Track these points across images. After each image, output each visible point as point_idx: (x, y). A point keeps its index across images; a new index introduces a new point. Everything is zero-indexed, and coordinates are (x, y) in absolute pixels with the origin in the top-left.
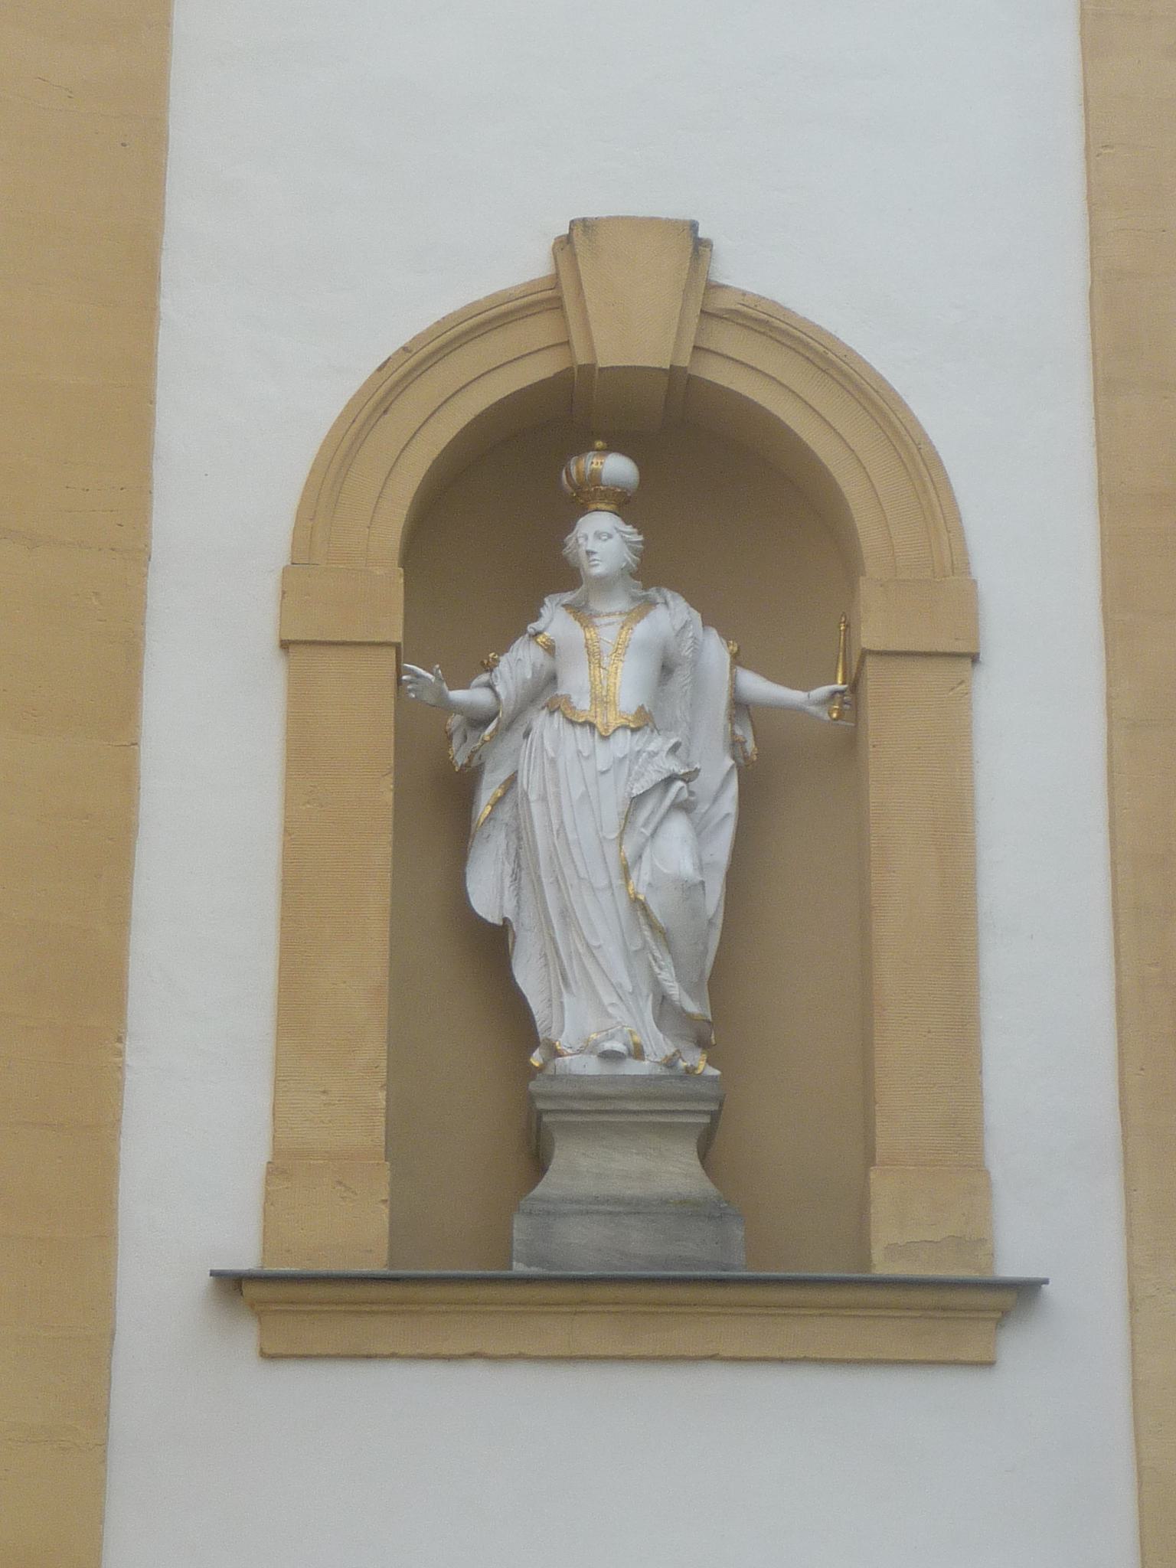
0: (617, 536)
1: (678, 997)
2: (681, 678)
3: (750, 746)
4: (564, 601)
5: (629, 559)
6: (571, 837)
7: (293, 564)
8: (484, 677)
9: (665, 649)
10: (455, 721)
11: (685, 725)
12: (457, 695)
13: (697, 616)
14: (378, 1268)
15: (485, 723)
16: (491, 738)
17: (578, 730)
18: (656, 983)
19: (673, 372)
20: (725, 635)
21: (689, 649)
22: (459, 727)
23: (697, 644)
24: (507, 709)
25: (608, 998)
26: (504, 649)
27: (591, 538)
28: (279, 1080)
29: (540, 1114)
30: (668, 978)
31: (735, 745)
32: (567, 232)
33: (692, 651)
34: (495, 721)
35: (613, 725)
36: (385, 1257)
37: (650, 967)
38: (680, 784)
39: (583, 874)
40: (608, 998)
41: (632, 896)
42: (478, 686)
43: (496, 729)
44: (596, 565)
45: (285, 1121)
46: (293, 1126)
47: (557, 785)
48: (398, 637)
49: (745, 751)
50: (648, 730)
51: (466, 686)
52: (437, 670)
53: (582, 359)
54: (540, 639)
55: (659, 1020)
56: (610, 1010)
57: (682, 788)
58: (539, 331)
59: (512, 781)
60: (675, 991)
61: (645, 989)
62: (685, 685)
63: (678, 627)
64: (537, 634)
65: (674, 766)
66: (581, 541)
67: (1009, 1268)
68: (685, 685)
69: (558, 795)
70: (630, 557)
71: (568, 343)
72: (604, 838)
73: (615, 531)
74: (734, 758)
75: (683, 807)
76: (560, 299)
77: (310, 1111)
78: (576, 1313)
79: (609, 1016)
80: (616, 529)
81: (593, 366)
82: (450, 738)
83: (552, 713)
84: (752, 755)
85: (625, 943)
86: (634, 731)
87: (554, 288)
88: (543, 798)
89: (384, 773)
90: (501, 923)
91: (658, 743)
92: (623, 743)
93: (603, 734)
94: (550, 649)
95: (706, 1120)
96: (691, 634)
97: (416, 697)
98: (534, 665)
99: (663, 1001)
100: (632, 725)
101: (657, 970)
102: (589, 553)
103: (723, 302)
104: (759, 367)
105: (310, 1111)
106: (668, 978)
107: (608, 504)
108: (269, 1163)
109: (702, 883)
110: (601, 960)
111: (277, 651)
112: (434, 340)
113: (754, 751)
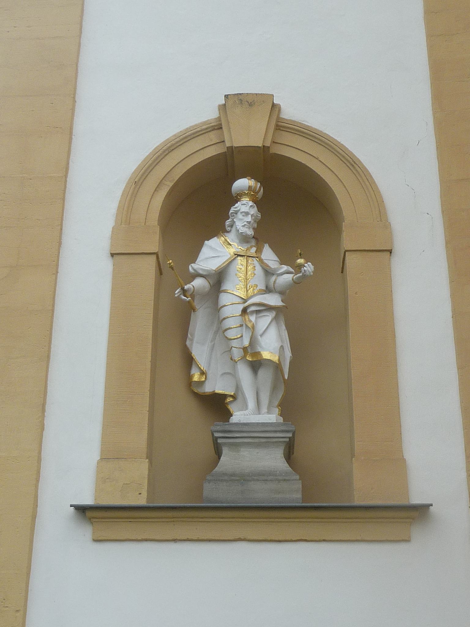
14: (142, 501)
19: (265, 148)
29: (217, 438)
53: (228, 144)
58: (213, 137)
67: (416, 500)
71: (224, 141)
76: (221, 124)
104: (289, 145)
111: (110, 258)
112: (339, 148)
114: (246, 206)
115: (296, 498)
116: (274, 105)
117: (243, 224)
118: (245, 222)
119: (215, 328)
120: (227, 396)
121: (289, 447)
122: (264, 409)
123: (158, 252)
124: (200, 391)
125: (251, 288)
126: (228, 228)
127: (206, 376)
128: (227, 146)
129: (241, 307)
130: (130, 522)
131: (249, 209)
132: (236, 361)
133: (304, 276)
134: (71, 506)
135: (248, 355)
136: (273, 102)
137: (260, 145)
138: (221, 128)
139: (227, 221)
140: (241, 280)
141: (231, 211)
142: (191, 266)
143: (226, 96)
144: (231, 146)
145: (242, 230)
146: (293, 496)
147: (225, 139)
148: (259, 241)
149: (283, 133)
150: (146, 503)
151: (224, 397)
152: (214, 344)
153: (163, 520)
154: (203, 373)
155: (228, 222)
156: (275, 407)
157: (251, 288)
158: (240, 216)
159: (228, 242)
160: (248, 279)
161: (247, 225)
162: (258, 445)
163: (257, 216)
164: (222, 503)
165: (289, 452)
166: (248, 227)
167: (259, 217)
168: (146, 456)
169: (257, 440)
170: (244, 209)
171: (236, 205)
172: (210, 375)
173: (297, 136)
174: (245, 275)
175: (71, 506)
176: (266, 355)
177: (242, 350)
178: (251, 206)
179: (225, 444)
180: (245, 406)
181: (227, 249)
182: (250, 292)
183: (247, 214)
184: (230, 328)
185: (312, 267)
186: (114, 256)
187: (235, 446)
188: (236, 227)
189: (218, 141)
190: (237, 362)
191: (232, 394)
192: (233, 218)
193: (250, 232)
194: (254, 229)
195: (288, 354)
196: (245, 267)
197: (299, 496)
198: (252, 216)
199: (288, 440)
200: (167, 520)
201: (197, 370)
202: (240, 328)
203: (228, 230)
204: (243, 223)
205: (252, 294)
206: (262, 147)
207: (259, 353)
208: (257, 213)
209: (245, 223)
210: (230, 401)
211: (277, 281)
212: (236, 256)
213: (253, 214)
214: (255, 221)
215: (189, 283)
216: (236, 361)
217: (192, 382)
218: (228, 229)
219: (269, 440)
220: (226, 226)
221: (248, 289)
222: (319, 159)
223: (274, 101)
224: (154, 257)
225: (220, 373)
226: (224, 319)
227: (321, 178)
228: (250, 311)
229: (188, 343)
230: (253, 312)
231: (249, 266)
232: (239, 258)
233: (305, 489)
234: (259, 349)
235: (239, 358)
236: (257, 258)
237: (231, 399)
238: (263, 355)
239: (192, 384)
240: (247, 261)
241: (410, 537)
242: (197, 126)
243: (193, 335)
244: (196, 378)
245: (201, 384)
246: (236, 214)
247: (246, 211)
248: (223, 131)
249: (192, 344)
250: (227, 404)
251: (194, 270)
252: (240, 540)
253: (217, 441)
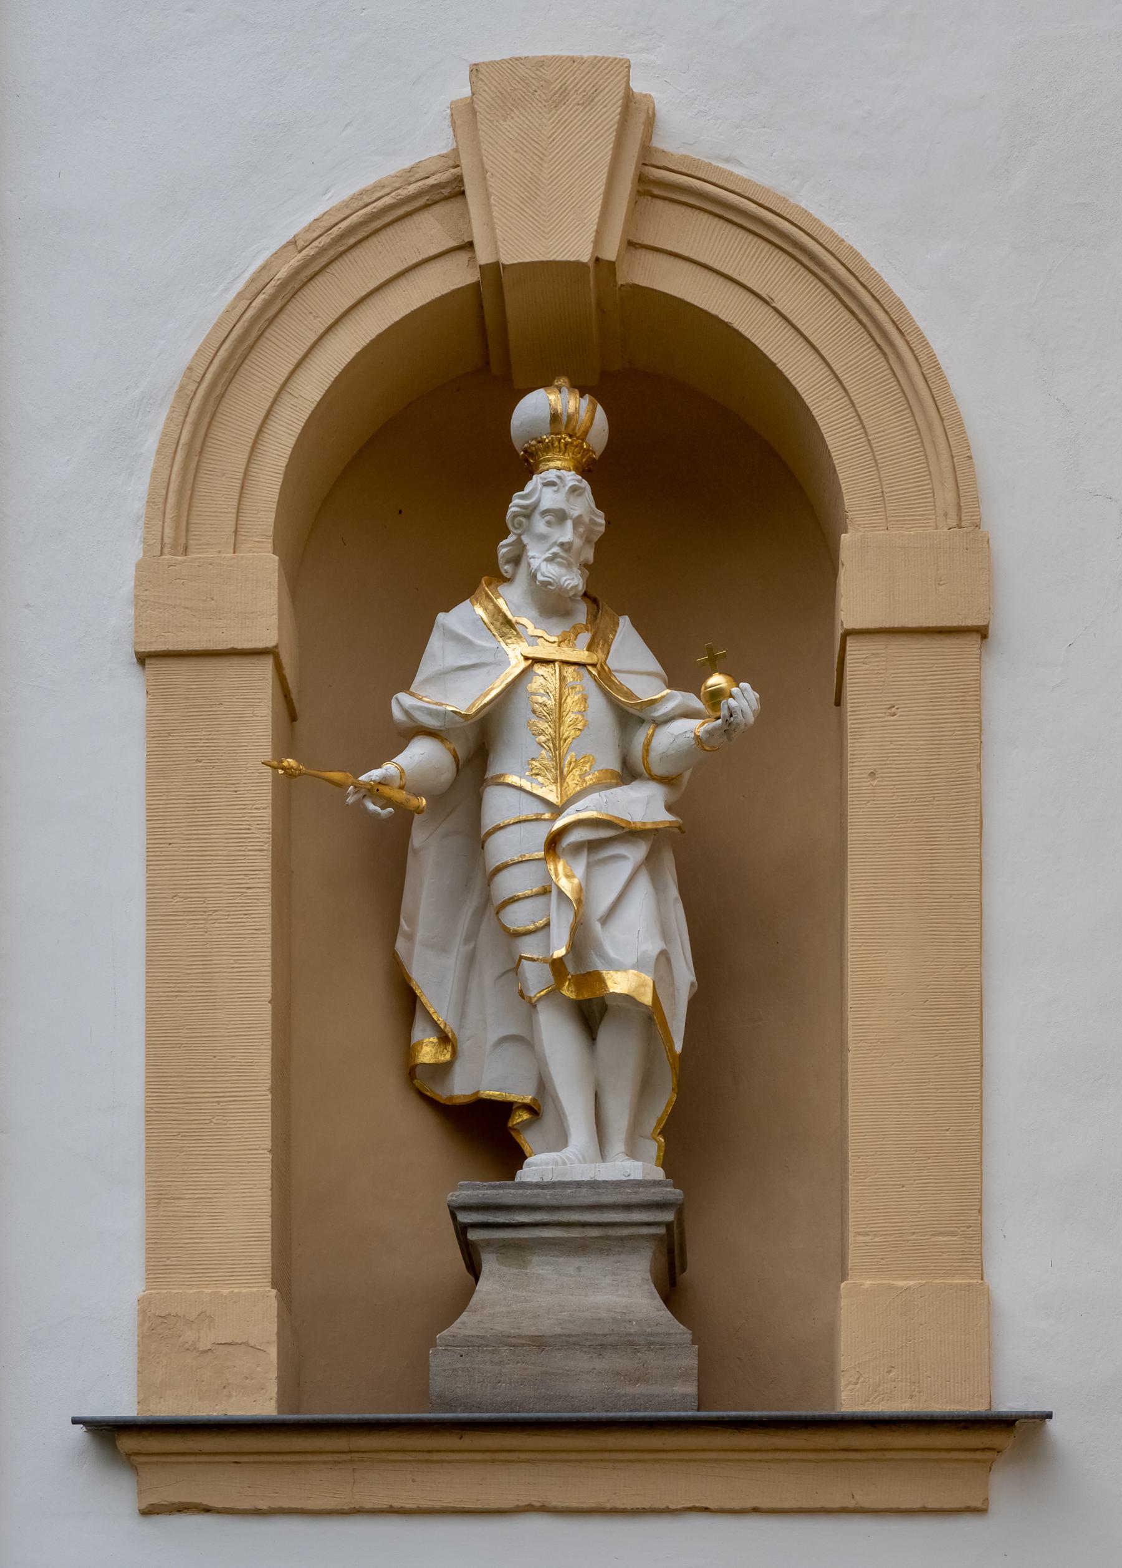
14: (266, 1407)
53: (484, 256)
67: (1008, 1404)
76: (459, 179)
111: (137, 669)
114: (555, 488)
115: (682, 1394)
116: (629, 101)
117: (548, 555)
118: (554, 544)
119: (473, 901)
120: (514, 1107)
121: (670, 1251)
122: (617, 1144)
123: (276, 647)
124: (441, 1093)
125: (573, 768)
126: (506, 567)
127: (453, 1046)
128: (482, 263)
129: (541, 833)
130: (236, 1465)
131: (568, 500)
132: (534, 1000)
133: (729, 728)
134: (75, 1421)
135: (565, 982)
136: (628, 88)
137: (585, 258)
138: (463, 193)
139: (501, 544)
140: (545, 743)
141: (512, 509)
142: (397, 699)
143: (475, 69)
145: (549, 571)
146: (673, 1390)
147: (473, 237)
148: (600, 606)
149: (660, 204)
151: (505, 1108)
152: (475, 947)
153: (325, 1458)
154: (445, 1039)
155: (504, 549)
156: (648, 1138)
157: (573, 768)
158: (540, 525)
159: (505, 616)
160: (565, 740)
161: (562, 557)
162: (581, 1248)
163: (593, 522)
164: (480, 1409)
165: (671, 1265)
166: (564, 561)
167: (601, 525)
168: (270, 1280)
169: (575, 1233)
170: (550, 499)
171: (529, 487)
172: (465, 1046)
173: (705, 217)
174: (557, 724)
175: (75, 1421)
176: (619, 983)
177: (547, 968)
178: (574, 490)
179: (488, 1243)
180: (562, 1140)
181: (500, 639)
182: (573, 783)
183: (560, 516)
184: (513, 900)
185: (753, 696)
187: (516, 1251)
188: (529, 565)
189: (453, 244)
190: (534, 1006)
191: (528, 1099)
192: (518, 532)
193: (573, 580)
194: (585, 566)
195: (685, 975)
196: (555, 700)
197: (691, 1389)
198: (577, 522)
199: (662, 1230)
200: (335, 1457)
201: (429, 1029)
202: (542, 900)
203: (505, 574)
204: (549, 550)
205: (578, 789)
206: (591, 265)
207: (596, 979)
208: (593, 512)
209: (556, 549)
210: (522, 1121)
211: (654, 743)
212: (530, 661)
213: (580, 516)
214: (588, 541)
215: (390, 757)
216: (534, 1000)
217: (417, 1065)
218: (506, 569)
219: (612, 1232)
220: (501, 561)
221: (565, 772)
222: (774, 305)
223: (631, 84)
224: (268, 664)
225: (493, 1037)
226: (499, 869)
227: (771, 366)
228: (568, 845)
229: (401, 945)
230: (577, 848)
231: (569, 694)
232: (539, 669)
233: (705, 1374)
234: (598, 964)
235: (542, 993)
236: (590, 668)
237: (526, 1116)
238: (609, 983)
239: (418, 1070)
240: (562, 679)
241: (986, 1501)
242: (384, 187)
243: (412, 922)
244: (428, 1052)
245: (442, 1070)
246: (528, 516)
247: (556, 506)
248: (466, 204)
249: (410, 952)
250: (515, 1129)
251: (407, 713)
252: (529, 1509)
253: (465, 1233)
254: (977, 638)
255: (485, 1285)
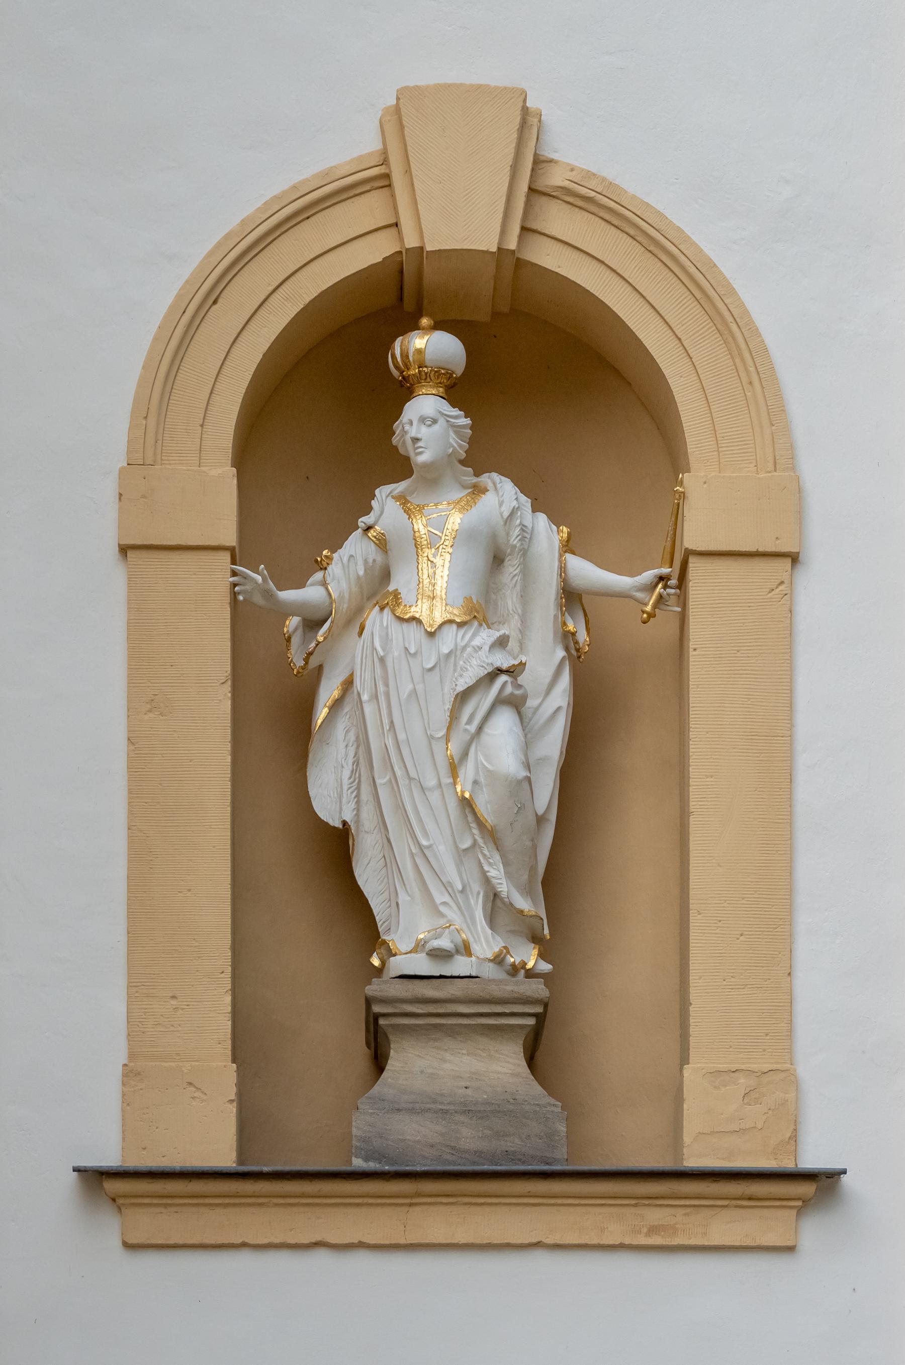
0: (442, 422)
1: (506, 894)
2: (511, 568)
3: (583, 636)
4: (395, 493)
5: (455, 445)
6: (402, 736)
7: (128, 464)
8: (319, 575)
9: (494, 537)
10: (293, 622)
11: (516, 617)
12: (288, 595)
13: (526, 502)
14: (227, 1160)
15: (321, 623)
16: (325, 638)
17: (405, 625)
18: (486, 881)
20: (556, 519)
21: (517, 537)
22: (296, 629)
23: (527, 533)
24: (342, 608)
25: (440, 897)
26: (336, 546)
27: (415, 423)
28: (131, 986)
29: (377, 1017)
30: (496, 873)
31: (567, 638)
32: (395, 102)
33: (520, 540)
34: (330, 619)
35: (439, 620)
36: (234, 1155)
37: (480, 863)
38: (503, 678)
39: (413, 774)
40: (440, 897)
41: (459, 794)
42: (312, 585)
43: (330, 629)
44: (421, 453)
45: (138, 1026)
46: (145, 1030)
47: (387, 685)
48: (231, 539)
49: (576, 643)
50: (476, 623)
51: (301, 585)
52: (262, 569)
53: (411, 242)
54: (372, 533)
55: (491, 921)
56: (442, 909)
57: (505, 683)
59: (348, 684)
60: (503, 887)
61: (476, 887)
62: (515, 575)
63: (506, 514)
64: (369, 528)
65: (503, 660)
66: (407, 427)
67: (809, 1161)
68: (515, 575)
69: (387, 694)
70: (457, 442)
72: (432, 737)
73: (439, 415)
74: (567, 649)
75: (516, 703)
76: (387, 176)
77: (162, 1015)
78: (411, 1205)
79: (442, 915)
80: (440, 412)
81: (421, 249)
82: (289, 640)
83: (382, 609)
84: (584, 646)
85: (455, 843)
86: (461, 625)
87: (382, 164)
88: (375, 697)
89: (222, 681)
90: (341, 827)
91: (486, 637)
92: (449, 639)
93: (429, 630)
94: (382, 544)
95: (531, 1021)
96: (518, 522)
97: (245, 599)
98: (366, 562)
99: (494, 899)
100: (458, 620)
101: (486, 868)
102: (416, 440)
103: (556, 178)
105: (162, 1015)
106: (496, 873)
107: (434, 387)
108: (125, 1065)
109: (528, 779)
110: (431, 860)
113: (585, 640)
116: (525, 111)
134: (74, 1170)
137: (494, 249)
144: (419, 247)
150: (234, 1165)
179: (393, 1026)
186: (130, 554)
254: (787, 562)
255: (394, 1063)
